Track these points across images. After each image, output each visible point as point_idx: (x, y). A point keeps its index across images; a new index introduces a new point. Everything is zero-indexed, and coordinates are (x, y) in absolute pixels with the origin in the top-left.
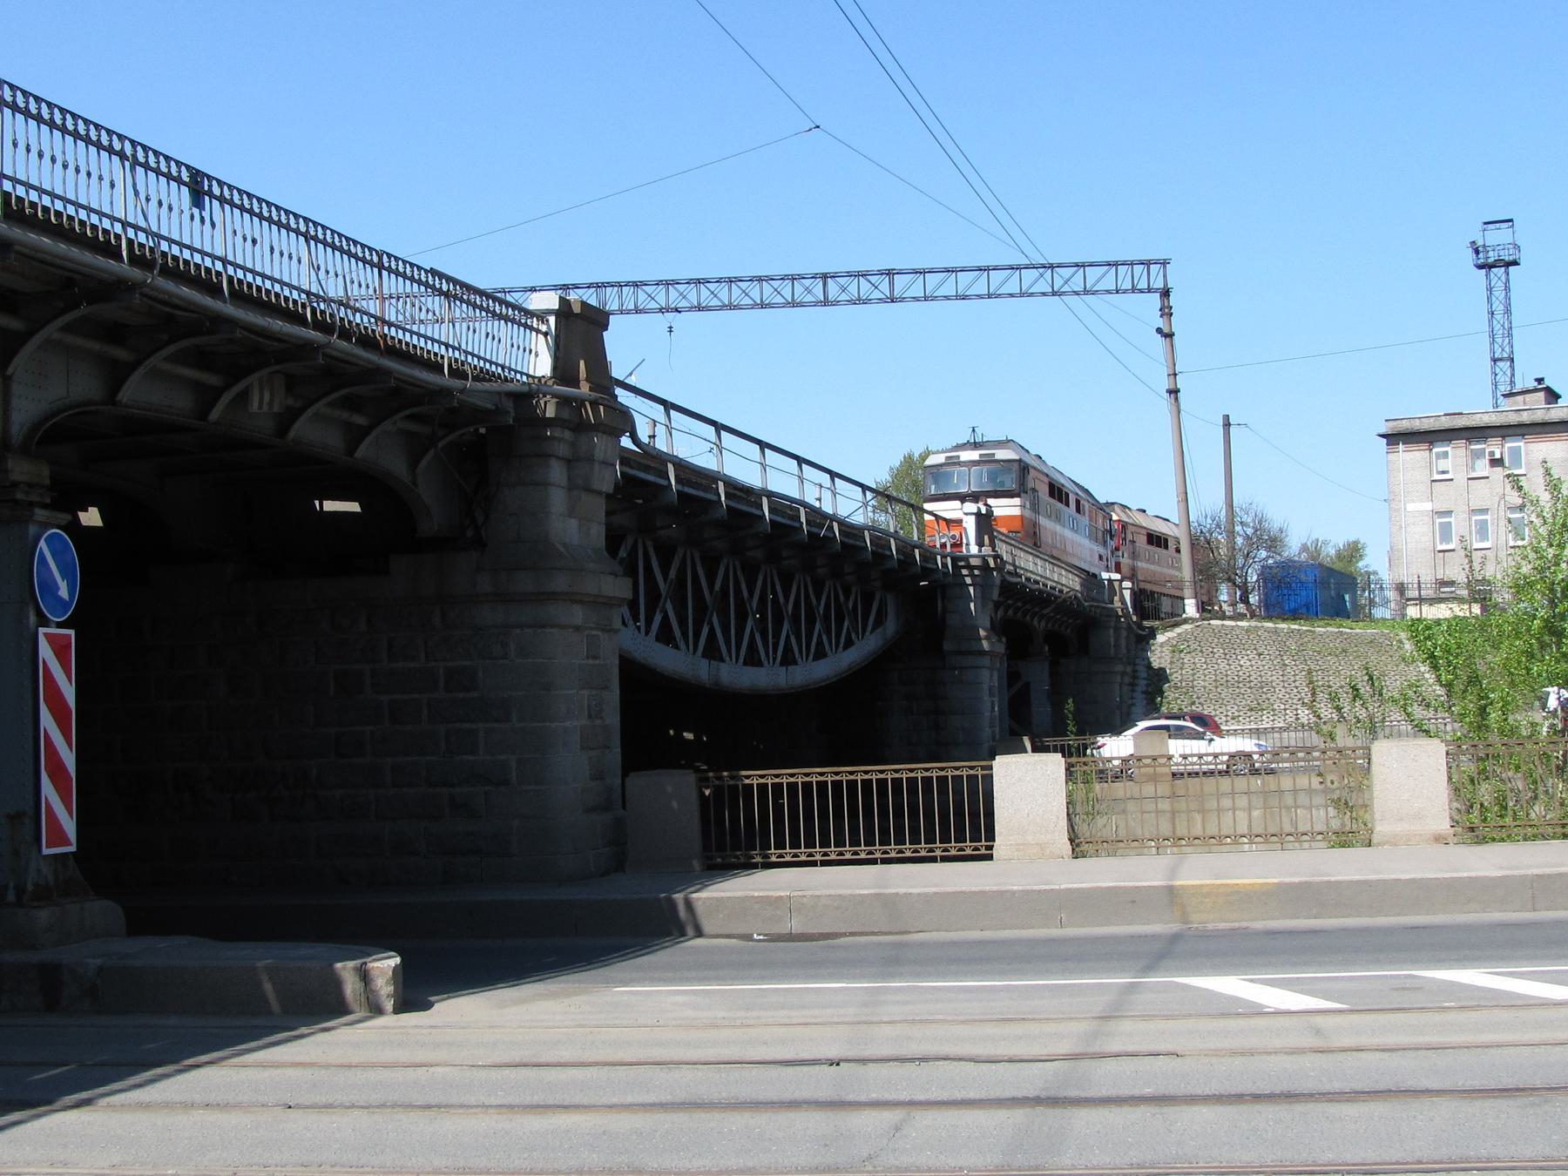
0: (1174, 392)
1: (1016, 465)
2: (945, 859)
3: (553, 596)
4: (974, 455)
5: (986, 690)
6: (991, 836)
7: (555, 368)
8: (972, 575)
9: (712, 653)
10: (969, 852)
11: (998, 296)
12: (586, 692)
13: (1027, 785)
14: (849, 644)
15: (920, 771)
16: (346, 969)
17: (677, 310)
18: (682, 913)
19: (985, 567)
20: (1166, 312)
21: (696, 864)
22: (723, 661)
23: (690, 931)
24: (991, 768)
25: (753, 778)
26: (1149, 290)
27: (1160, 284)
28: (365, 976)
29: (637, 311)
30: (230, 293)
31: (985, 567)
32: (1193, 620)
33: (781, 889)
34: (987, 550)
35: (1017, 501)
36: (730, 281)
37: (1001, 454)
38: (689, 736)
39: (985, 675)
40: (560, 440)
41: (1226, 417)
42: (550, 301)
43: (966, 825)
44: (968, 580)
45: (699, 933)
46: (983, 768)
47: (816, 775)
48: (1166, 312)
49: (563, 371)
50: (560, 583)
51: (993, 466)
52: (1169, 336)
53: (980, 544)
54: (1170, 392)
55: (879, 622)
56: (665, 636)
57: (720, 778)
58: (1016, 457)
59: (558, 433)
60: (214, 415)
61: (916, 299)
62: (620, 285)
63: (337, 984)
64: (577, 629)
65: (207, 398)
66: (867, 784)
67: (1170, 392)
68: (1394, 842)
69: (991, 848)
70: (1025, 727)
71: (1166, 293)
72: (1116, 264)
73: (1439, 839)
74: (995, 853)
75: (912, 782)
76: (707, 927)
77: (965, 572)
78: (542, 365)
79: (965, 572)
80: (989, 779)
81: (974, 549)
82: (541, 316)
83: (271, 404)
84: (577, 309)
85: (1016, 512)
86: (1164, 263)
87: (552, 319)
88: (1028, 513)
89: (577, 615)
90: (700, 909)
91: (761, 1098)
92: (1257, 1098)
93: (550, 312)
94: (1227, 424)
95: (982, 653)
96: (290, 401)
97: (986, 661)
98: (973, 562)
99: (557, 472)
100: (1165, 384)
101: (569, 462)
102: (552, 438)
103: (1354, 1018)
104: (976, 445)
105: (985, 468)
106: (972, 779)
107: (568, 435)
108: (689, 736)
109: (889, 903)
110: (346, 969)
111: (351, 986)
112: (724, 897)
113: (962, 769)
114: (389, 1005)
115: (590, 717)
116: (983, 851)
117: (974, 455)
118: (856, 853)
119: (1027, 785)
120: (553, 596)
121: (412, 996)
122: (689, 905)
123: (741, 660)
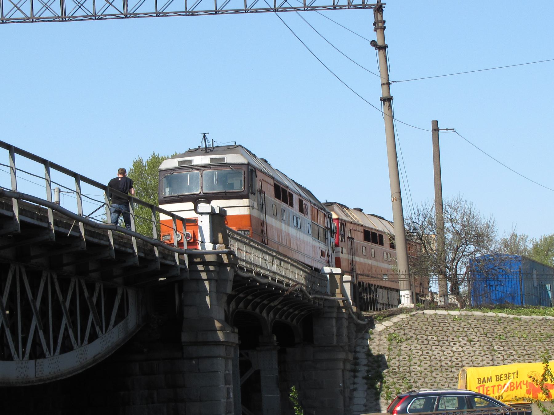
0: (387, 100)
8: (207, 271)
14: (93, 337)
19: (219, 263)
20: (380, 26)
31: (219, 263)
34: (220, 247)
37: (231, 158)
44: (204, 276)
51: (222, 170)
52: (383, 48)
53: (214, 241)
54: (384, 100)
55: (121, 316)
61: (148, 15)
67: (384, 100)
71: (379, 9)
77: (200, 268)
85: (245, 211)
88: (256, 213)
95: (218, 343)
97: (221, 351)
98: (209, 258)
100: (380, 93)
104: (207, 151)
105: (216, 172)
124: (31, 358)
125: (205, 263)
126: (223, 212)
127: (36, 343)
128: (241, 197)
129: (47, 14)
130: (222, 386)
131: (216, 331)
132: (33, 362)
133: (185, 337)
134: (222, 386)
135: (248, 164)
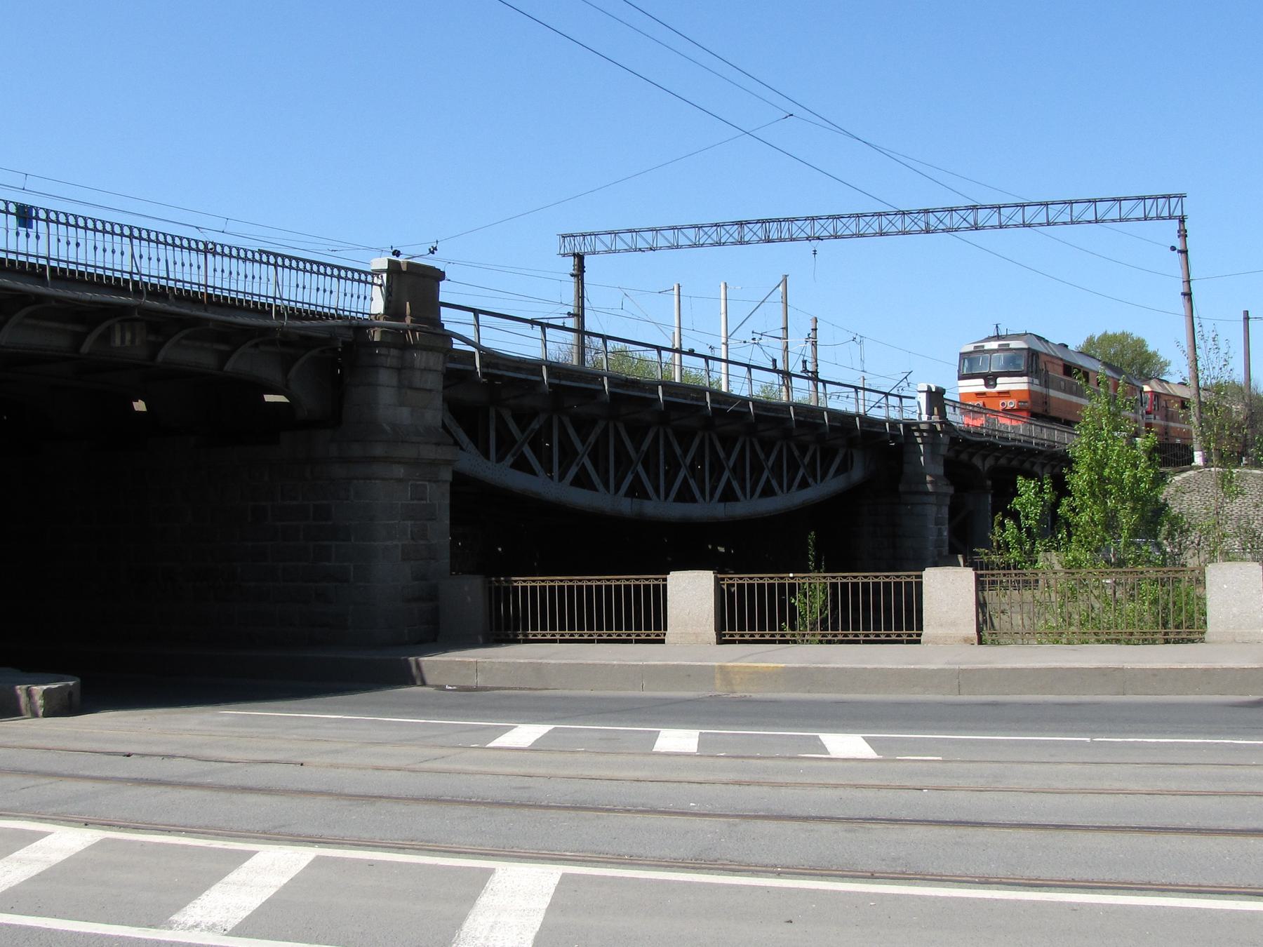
0: (1188, 295)
1: (1025, 353)
2: (600, 641)
3: (375, 459)
4: (994, 345)
5: (934, 521)
6: (920, 627)
7: (386, 308)
8: (922, 436)
9: (636, 491)
10: (653, 637)
11: (1128, 220)
12: (409, 523)
13: (947, 591)
14: (804, 484)
15: (882, 577)
16: (20, 690)
17: (818, 238)
18: (414, 670)
19: (932, 427)
20: (1183, 234)
21: (480, 639)
22: (649, 498)
23: (419, 683)
24: (921, 577)
25: (520, 582)
26: (1170, 218)
27: (1178, 213)
28: (29, 694)
29: (792, 240)
30: (51, 277)
31: (932, 427)
32: (1198, 467)
33: (518, 658)
34: (935, 418)
35: (1025, 379)
36: (858, 216)
37: (1014, 344)
38: (722, 550)
39: (931, 511)
40: (387, 356)
41: (1246, 313)
42: (381, 263)
43: (900, 618)
44: (919, 440)
45: (424, 684)
46: (917, 577)
47: (558, 581)
48: (1183, 234)
49: (392, 308)
50: (379, 450)
51: (1008, 354)
52: (1184, 252)
53: (930, 413)
54: (1184, 294)
55: (844, 468)
56: (582, 481)
57: (499, 581)
58: (1025, 346)
59: (384, 351)
60: (85, 349)
61: (993, 227)
62: (778, 221)
63: (16, 698)
64: (399, 480)
65: (79, 339)
66: (589, 588)
67: (1184, 294)
68: (1214, 642)
69: (919, 635)
70: (962, 544)
71: (1182, 220)
72: (1144, 198)
73: (967, 640)
74: (922, 639)
75: (876, 585)
76: (429, 680)
77: (917, 434)
78: (377, 305)
79: (917, 434)
80: (919, 585)
81: (925, 418)
82: (376, 273)
83: (133, 341)
84: (404, 268)
85: (1025, 387)
86: (1181, 196)
87: (385, 276)
88: (1037, 388)
89: (400, 471)
90: (424, 669)
91: (794, 814)
92: (397, 799)
93: (382, 271)
94: (1247, 318)
95: (927, 493)
96: (152, 338)
97: (932, 499)
98: (923, 427)
99: (385, 377)
100: (1181, 288)
101: (399, 370)
102: (379, 354)
103: (884, 764)
104: (998, 337)
105: (1002, 355)
106: (909, 584)
107: (394, 352)
108: (722, 550)
109: (538, 669)
110: (20, 690)
111: (23, 700)
112: (434, 664)
113: (904, 576)
114: (41, 711)
115: (413, 539)
116: (915, 637)
117: (994, 345)
118: (888, 635)
119: (947, 591)
120: (375, 459)
121: (61, 707)
122: (418, 665)
123: (673, 495)
124: (720, 500)
125: (921, 431)
126: (987, 385)
127: (729, 488)
128: (1021, 376)
129: (916, 228)
130: (931, 526)
131: (925, 483)
132: (722, 505)
133: (901, 488)
134: (931, 526)
135: (1029, 349)
